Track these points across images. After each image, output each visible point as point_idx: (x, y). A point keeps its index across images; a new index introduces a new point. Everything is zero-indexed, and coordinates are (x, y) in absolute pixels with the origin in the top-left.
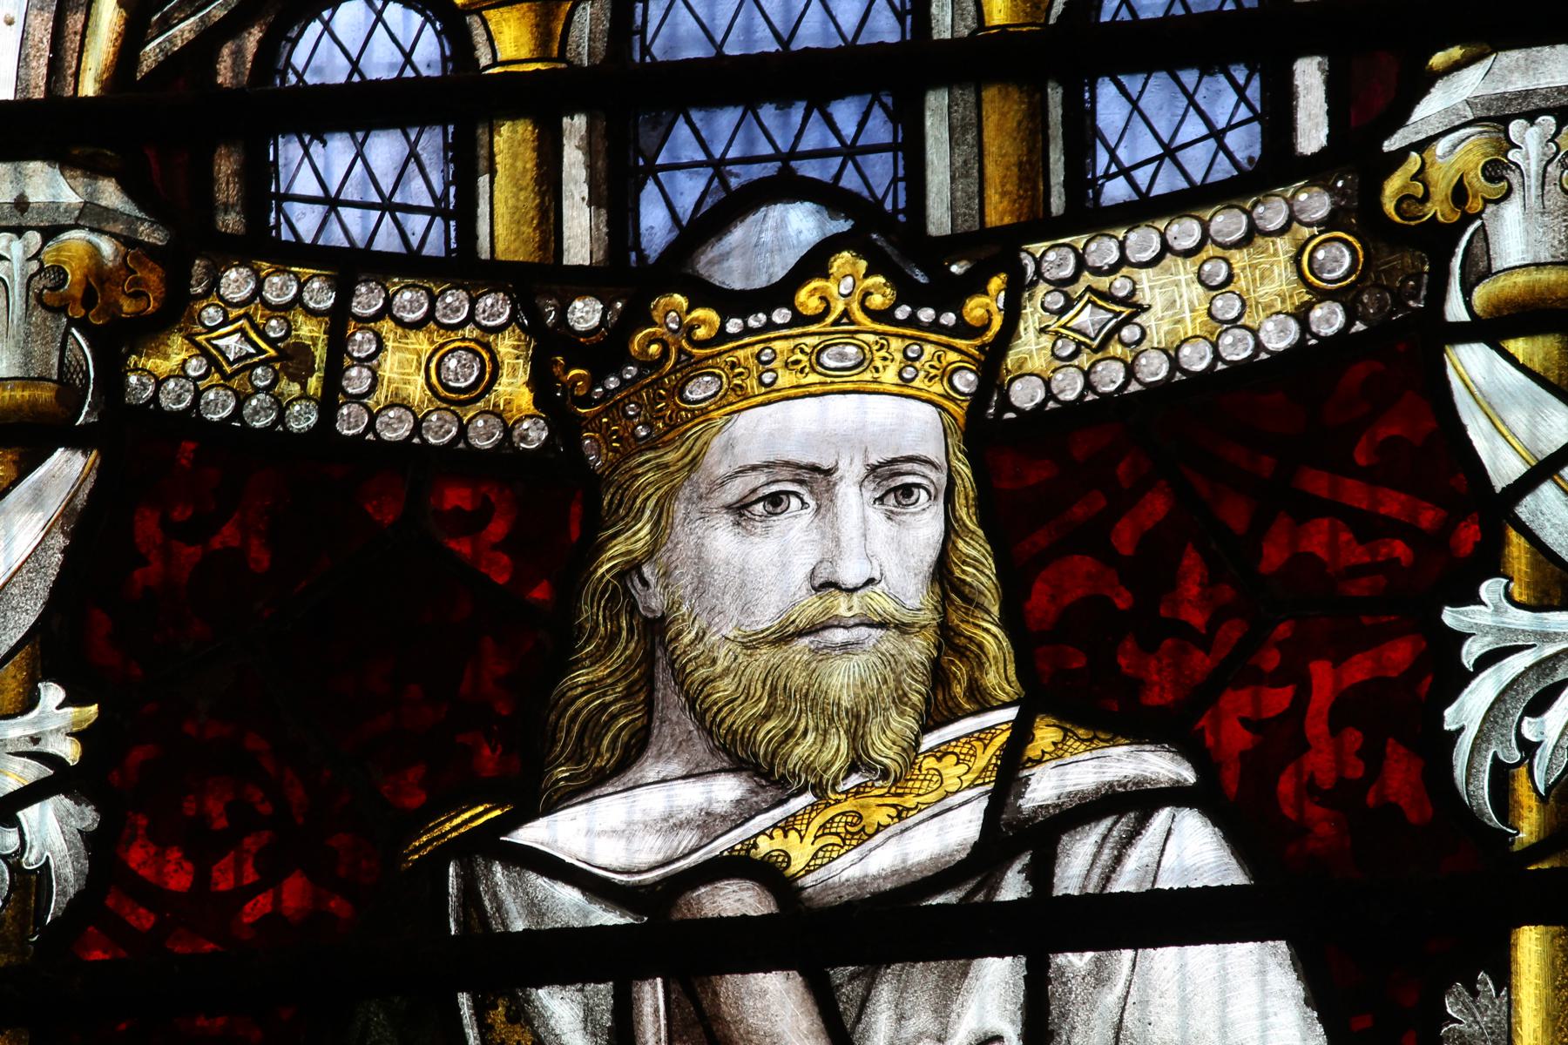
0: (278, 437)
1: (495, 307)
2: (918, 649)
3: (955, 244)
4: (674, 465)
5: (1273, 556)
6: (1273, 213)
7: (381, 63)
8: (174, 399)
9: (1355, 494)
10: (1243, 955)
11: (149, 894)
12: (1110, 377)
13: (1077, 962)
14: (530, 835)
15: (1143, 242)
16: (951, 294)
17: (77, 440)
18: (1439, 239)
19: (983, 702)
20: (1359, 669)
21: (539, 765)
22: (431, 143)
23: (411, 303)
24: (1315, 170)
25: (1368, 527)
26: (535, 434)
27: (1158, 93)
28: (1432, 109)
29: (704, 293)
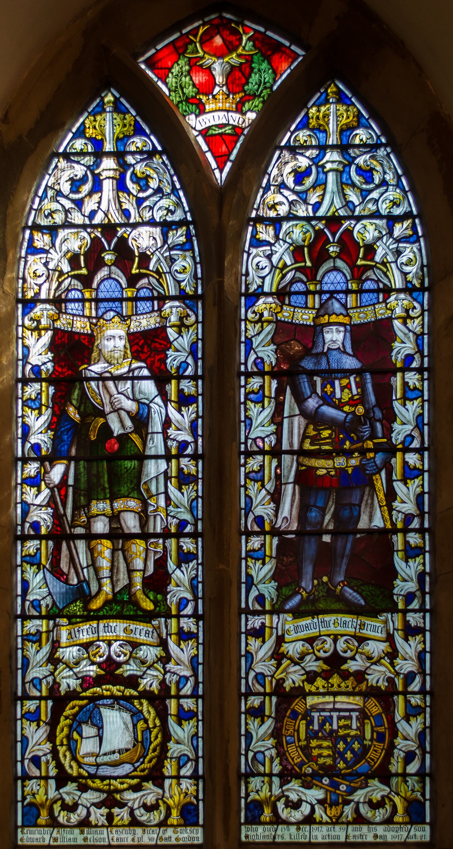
0: (67, 331)
1: (86, 320)
2: (122, 353)
3: (126, 316)
4: (69, 737)
5: (152, 346)
6: (153, 315)
7: (76, 297)
8: (59, 327)
9: (159, 341)
10: (149, 381)
11: (58, 371)
12: (139, 330)
13: (136, 381)
14: (90, 368)
15: (141, 317)
16: (125, 321)
17: (51, 330)
18: (166, 318)
19: (128, 358)
20: (159, 357)
21: (90, 362)
22: (80, 304)
23: (79, 319)
24: (156, 311)
25: (160, 344)
26: (90, 332)
27: (143, 303)
28: (166, 306)
29: (104, 319)
